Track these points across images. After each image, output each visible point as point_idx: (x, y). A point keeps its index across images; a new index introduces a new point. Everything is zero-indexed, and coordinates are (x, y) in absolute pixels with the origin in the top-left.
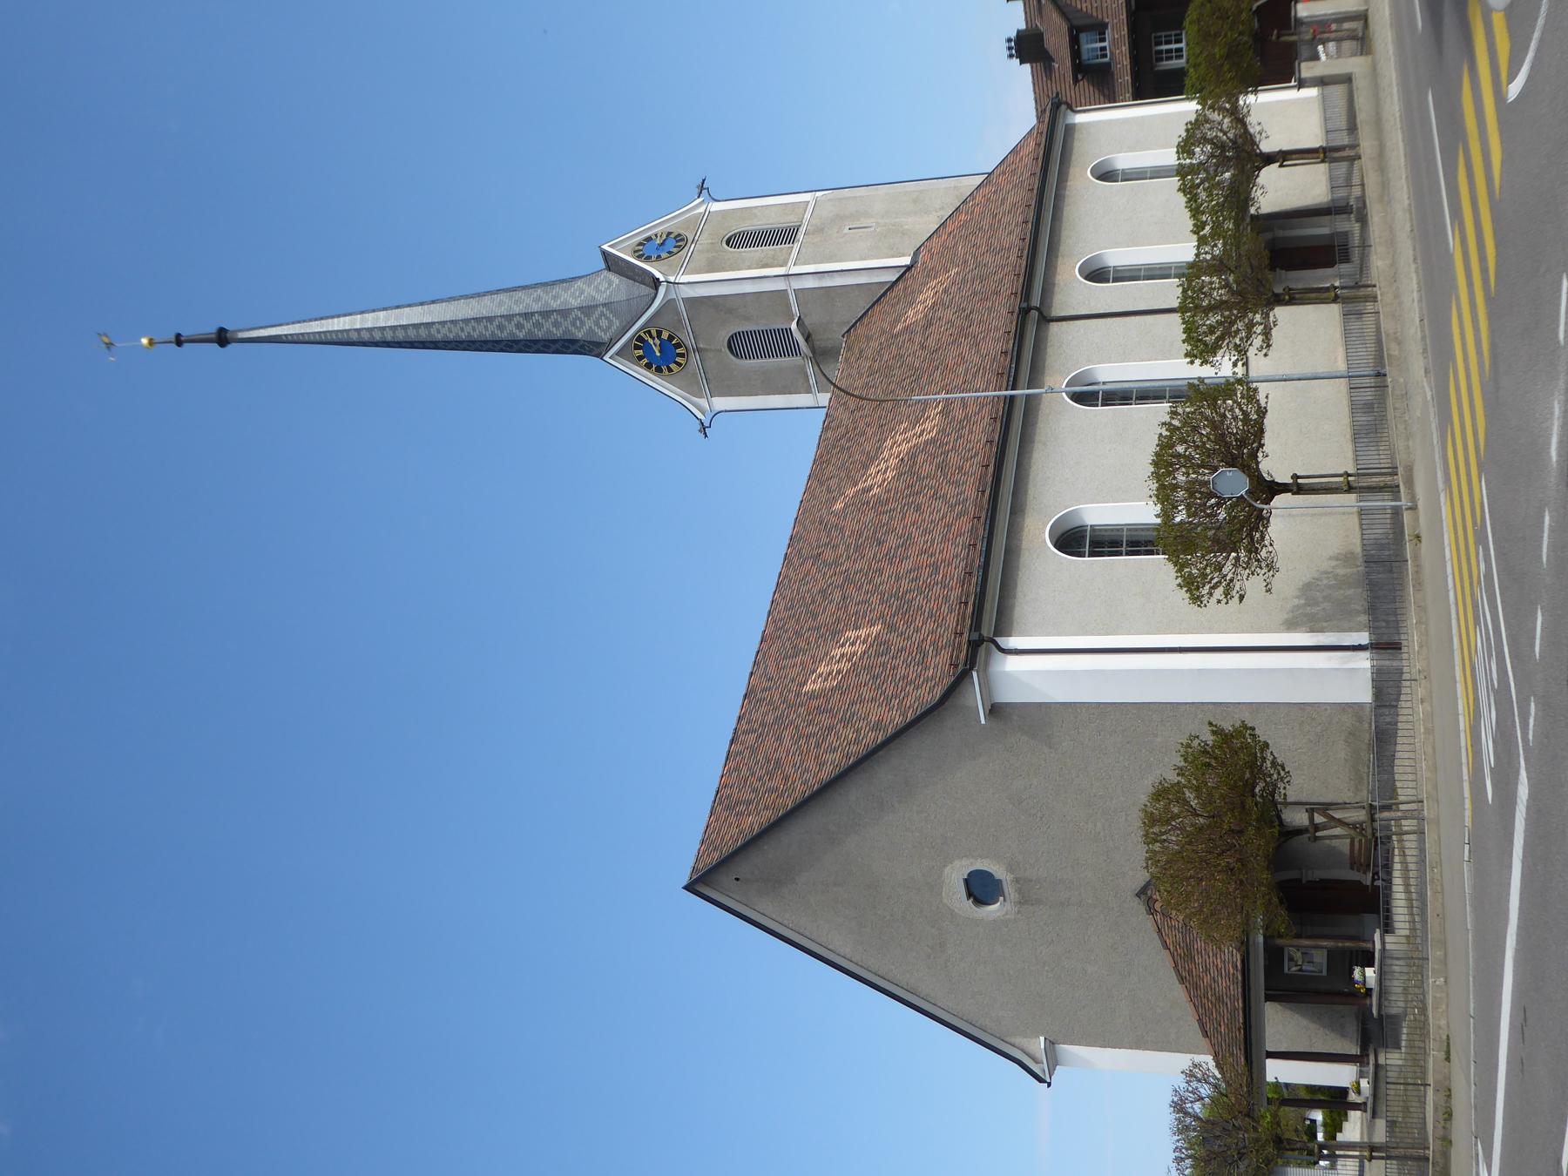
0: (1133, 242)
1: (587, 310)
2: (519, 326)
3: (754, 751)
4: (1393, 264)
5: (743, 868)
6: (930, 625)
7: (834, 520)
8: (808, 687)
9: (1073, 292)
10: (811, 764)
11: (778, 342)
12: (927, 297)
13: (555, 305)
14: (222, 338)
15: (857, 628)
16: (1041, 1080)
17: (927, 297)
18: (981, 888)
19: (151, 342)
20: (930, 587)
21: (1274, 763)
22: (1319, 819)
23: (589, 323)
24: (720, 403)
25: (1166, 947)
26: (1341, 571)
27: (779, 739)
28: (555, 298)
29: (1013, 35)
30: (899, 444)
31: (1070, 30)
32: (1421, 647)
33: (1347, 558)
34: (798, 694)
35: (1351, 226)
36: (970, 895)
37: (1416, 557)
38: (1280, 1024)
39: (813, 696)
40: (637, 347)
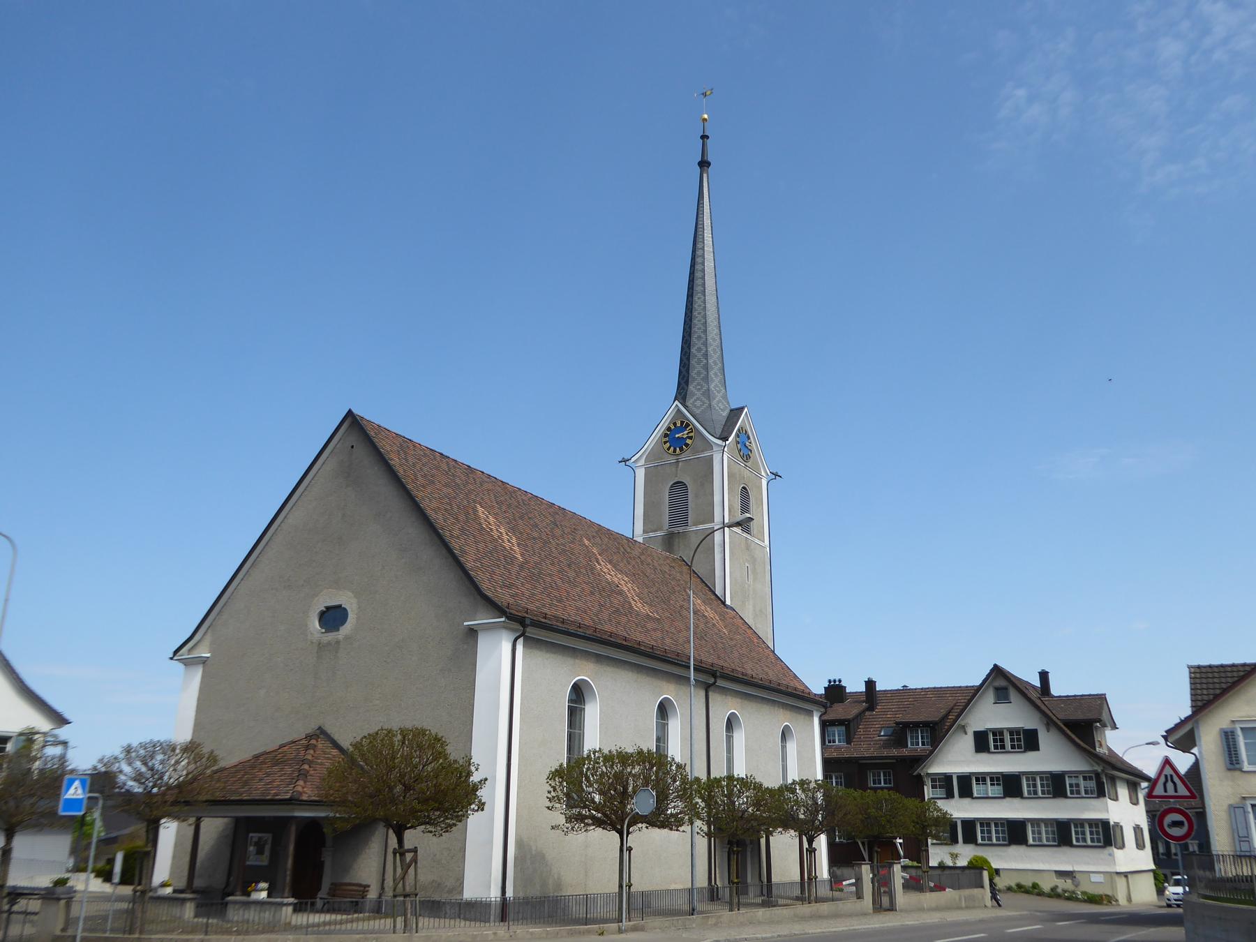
0: (748, 750)
1: (708, 394)
2: (699, 350)
3: (437, 468)
4: (760, 923)
5: (361, 452)
6: (527, 593)
7: (578, 538)
8: (480, 509)
9: (723, 707)
10: (434, 504)
11: (679, 513)
12: (709, 613)
13: (711, 374)
14: (704, 164)
15: (519, 545)
16: (176, 652)
17: (709, 613)
18: (333, 617)
19: (705, 120)
20: (548, 595)
21: (451, 826)
22: (409, 856)
23: (698, 394)
24: (641, 474)
25: (282, 746)
26: (551, 881)
27: (446, 485)
28: (716, 374)
29: (843, 684)
30: (627, 586)
31: (849, 721)
32: (532, 933)
33: (559, 886)
34: (474, 501)
35: (753, 895)
36: (328, 608)
37: (589, 932)
38: (213, 827)
39: (475, 510)
40: (682, 423)
